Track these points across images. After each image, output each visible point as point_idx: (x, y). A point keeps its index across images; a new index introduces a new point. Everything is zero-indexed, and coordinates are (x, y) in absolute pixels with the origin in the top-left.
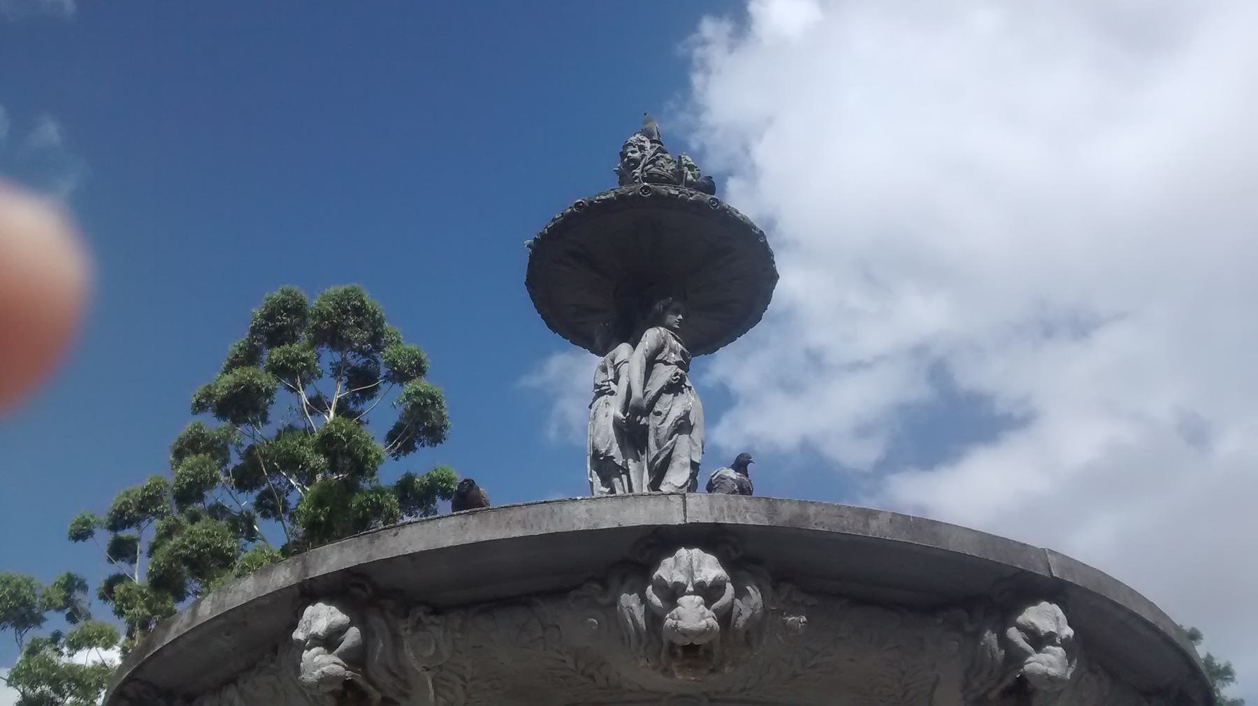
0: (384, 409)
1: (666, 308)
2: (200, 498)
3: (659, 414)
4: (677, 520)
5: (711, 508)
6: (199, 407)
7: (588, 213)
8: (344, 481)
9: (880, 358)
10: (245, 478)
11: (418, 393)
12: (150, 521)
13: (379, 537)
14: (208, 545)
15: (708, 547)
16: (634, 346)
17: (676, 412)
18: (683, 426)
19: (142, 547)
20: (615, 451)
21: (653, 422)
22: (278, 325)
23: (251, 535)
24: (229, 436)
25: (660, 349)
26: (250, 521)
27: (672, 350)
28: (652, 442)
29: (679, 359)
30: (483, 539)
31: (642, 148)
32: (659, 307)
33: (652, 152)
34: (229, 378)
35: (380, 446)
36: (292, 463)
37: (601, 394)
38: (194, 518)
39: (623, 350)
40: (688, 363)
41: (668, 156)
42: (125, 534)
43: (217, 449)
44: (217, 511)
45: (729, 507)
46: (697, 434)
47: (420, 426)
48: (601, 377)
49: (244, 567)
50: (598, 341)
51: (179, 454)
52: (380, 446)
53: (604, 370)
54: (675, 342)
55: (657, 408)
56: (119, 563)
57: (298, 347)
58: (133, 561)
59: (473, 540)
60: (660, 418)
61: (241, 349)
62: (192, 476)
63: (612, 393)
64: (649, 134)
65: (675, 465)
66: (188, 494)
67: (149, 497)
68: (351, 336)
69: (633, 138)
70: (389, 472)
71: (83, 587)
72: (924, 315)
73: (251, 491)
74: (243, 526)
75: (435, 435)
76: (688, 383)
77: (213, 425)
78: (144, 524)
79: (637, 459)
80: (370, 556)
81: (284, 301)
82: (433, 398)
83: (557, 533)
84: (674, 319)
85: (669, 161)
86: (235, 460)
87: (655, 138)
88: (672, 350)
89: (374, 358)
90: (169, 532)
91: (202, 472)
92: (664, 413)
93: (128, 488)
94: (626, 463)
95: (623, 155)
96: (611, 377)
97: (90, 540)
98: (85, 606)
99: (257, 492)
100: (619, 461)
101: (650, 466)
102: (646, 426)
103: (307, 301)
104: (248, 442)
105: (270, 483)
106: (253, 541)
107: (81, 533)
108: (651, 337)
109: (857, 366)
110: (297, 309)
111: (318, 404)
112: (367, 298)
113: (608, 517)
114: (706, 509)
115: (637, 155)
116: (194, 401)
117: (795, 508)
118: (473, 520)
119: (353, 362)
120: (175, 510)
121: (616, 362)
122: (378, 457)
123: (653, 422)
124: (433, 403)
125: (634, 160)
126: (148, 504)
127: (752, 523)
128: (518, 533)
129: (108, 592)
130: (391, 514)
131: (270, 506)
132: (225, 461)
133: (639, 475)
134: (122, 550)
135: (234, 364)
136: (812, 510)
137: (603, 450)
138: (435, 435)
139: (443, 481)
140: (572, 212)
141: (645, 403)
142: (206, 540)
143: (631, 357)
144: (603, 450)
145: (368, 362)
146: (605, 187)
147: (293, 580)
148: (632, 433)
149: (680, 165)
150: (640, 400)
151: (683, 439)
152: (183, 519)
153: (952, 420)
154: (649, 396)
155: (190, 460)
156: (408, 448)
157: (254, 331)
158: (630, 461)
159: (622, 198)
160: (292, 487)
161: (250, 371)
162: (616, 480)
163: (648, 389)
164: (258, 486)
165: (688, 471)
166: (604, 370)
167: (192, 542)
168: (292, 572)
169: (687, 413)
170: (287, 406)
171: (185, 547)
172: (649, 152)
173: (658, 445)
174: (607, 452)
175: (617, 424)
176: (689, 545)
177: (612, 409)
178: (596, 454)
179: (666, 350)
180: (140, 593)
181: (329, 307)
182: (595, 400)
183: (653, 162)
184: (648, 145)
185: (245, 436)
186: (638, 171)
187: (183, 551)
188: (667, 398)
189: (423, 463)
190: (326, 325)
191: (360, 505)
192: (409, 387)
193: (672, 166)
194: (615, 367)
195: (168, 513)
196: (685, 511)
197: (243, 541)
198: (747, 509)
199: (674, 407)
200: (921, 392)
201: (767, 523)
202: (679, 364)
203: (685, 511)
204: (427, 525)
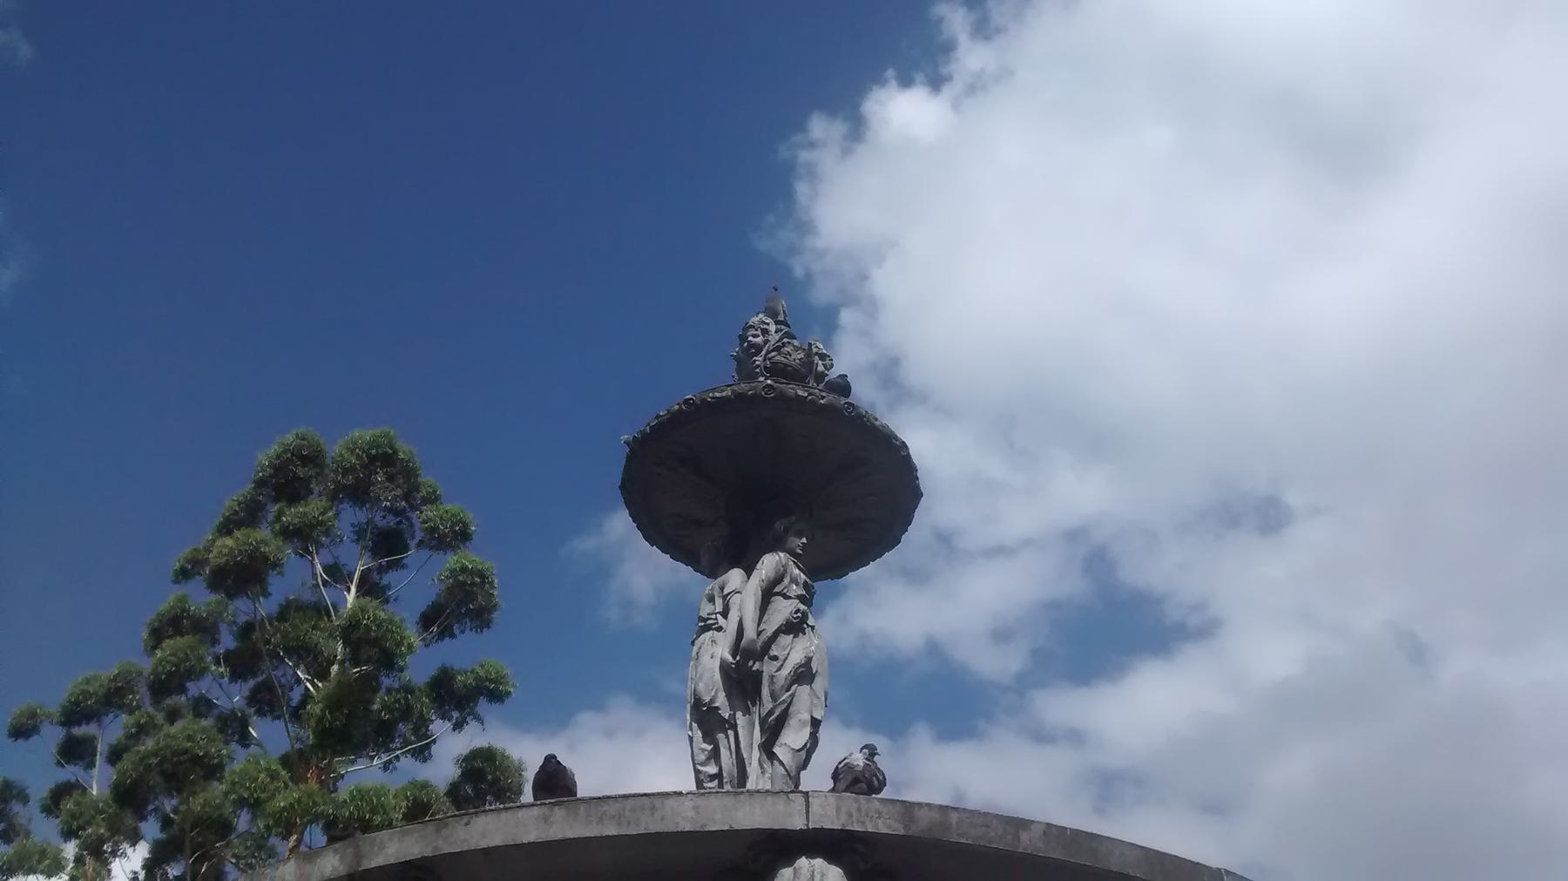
0: (419, 580)
1: (787, 530)
2: (182, 690)
3: (775, 658)
4: (798, 823)
5: (838, 810)
6: (184, 575)
7: (697, 413)
8: (367, 674)
9: (1027, 543)
10: (241, 664)
11: (464, 569)
13: (447, 825)
14: (186, 752)
15: (832, 858)
16: (749, 572)
17: (796, 657)
18: (804, 674)
19: (101, 748)
20: (721, 701)
21: (768, 668)
22: (288, 480)
23: (245, 740)
24: (221, 613)
25: (779, 579)
26: (244, 724)
27: (794, 581)
28: (765, 692)
29: (801, 592)
30: (570, 835)
31: (765, 332)
32: (779, 526)
35: (413, 635)
36: (306, 653)
37: (707, 628)
38: (173, 716)
39: (735, 577)
40: (812, 595)
41: (796, 343)
42: (79, 731)
43: (205, 629)
44: (202, 706)
45: (859, 810)
46: (819, 684)
47: (463, 606)
49: (234, 783)
50: (705, 561)
51: (157, 636)
52: (413, 635)
53: (711, 599)
54: (797, 571)
55: (774, 651)
56: (70, 768)
57: (314, 507)
58: (91, 765)
59: (559, 836)
60: (777, 664)
63: (720, 629)
64: (773, 314)
65: (793, 722)
66: (165, 685)
67: (118, 690)
68: (384, 498)
69: (755, 320)
70: (421, 663)
71: (24, 799)
72: (1082, 493)
73: (245, 680)
75: (482, 617)
76: (811, 621)
77: (200, 598)
78: (107, 720)
79: (747, 712)
80: (436, 848)
81: (300, 448)
82: (482, 575)
83: (658, 833)
84: (799, 542)
85: (797, 349)
86: (227, 641)
87: (781, 318)
88: (794, 581)
89: (408, 519)
90: (141, 731)
91: (187, 659)
92: (782, 658)
93: (90, 673)
94: (733, 716)
95: (743, 338)
96: (719, 608)
97: (34, 739)
98: (23, 821)
99: (252, 683)
100: (726, 713)
101: (763, 722)
102: (760, 673)
103: (326, 448)
104: (242, 619)
105: (268, 671)
106: (246, 746)
107: (22, 730)
108: (769, 564)
109: (1000, 551)
110: (309, 456)
111: (337, 574)
112: (399, 444)
113: (718, 816)
114: (832, 811)
115: (759, 340)
116: (178, 565)
117: (935, 815)
118: (559, 813)
119: (381, 523)
120: (147, 701)
122: (410, 647)
123: (768, 668)
124: (483, 583)
126: (114, 697)
127: (884, 831)
128: (611, 830)
129: (53, 805)
130: (421, 716)
131: (266, 700)
132: (215, 642)
133: (749, 732)
134: (75, 751)
135: (226, 528)
136: (954, 818)
137: (707, 699)
138: (482, 617)
139: (492, 681)
140: (680, 410)
141: (759, 644)
143: (743, 587)
144: (707, 699)
145: (400, 522)
146: (719, 380)
147: (342, 870)
148: (742, 679)
149: (809, 353)
150: (753, 641)
151: (803, 691)
152: (160, 718)
153: (1109, 623)
154: (764, 637)
155: (168, 644)
156: (446, 633)
157: (260, 484)
158: (739, 714)
159: (740, 397)
160: (299, 681)
162: (721, 736)
164: (254, 675)
165: (807, 730)
166: (711, 599)
168: (342, 860)
169: (809, 660)
170: (297, 576)
172: (774, 338)
173: (774, 697)
174: (712, 701)
175: (724, 667)
176: (811, 854)
177: (716, 650)
178: (697, 703)
179: (786, 581)
183: (777, 349)
184: (772, 328)
185: (241, 609)
186: (759, 359)
188: (785, 640)
189: (465, 653)
191: (385, 707)
192: (452, 560)
194: (724, 597)
195: (138, 707)
196: (807, 813)
197: (234, 746)
198: (880, 814)
199: (794, 651)
200: (1074, 586)
201: (902, 832)
202: (801, 598)
203: (807, 813)
204: (504, 815)
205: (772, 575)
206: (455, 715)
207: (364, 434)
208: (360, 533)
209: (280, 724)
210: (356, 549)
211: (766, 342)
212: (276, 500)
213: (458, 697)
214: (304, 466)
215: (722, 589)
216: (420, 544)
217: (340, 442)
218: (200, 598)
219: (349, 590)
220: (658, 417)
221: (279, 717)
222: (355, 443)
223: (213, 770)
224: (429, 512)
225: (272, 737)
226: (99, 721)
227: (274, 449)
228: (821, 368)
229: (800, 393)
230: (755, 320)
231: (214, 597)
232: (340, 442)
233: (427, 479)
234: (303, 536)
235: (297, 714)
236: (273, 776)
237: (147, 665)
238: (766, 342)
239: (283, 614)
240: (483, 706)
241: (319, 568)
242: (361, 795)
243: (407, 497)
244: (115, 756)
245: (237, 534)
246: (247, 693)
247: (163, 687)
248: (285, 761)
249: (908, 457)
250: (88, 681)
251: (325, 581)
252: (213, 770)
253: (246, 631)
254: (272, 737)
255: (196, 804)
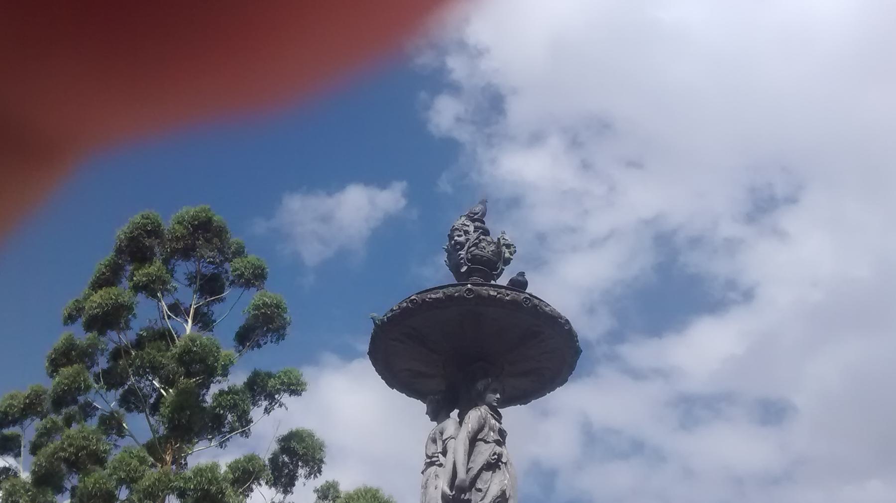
2: (75, 402)
3: (480, 490)
6: (70, 319)
10: (111, 379)
11: (265, 304)
12: (33, 420)
14: (84, 448)
22: (135, 249)
23: (121, 432)
25: (481, 429)
27: (491, 429)
29: (497, 437)
32: (480, 386)
33: (475, 236)
34: (97, 298)
35: (228, 350)
37: (430, 464)
38: (68, 422)
41: (489, 239)
43: (86, 356)
48: (432, 449)
49: (115, 468)
51: (55, 364)
52: (228, 350)
55: (479, 485)
57: (155, 267)
61: (106, 267)
62: (66, 385)
63: (441, 465)
67: (31, 403)
74: (112, 425)
77: (82, 337)
81: (145, 225)
85: (489, 243)
86: (103, 363)
88: (491, 429)
92: (484, 490)
93: (13, 392)
95: (451, 237)
96: (440, 450)
99: (121, 391)
104: (111, 346)
106: (123, 437)
110: (155, 232)
121: (444, 437)
125: (457, 243)
131: (131, 401)
135: (100, 284)
140: (408, 306)
142: (84, 443)
150: (464, 481)
155: (66, 371)
157: (119, 251)
160: (155, 390)
161: (114, 290)
163: (471, 465)
164: (122, 384)
167: (70, 445)
170: (147, 313)
171: (64, 450)
172: (473, 236)
179: (486, 430)
180: (24, 487)
181: (180, 230)
182: (425, 470)
183: (476, 245)
185: (113, 339)
186: (463, 253)
187: (62, 454)
188: (487, 475)
189: (267, 357)
190: (181, 245)
192: (254, 297)
193: (493, 248)
194: (444, 441)
205: (476, 427)
206: (265, 403)
207: (188, 211)
208: (191, 279)
209: (143, 415)
210: (190, 290)
211: (468, 240)
212: (132, 262)
213: (261, 388)
214: (149, 237)
215: (442, 434)
216: (232, 283)
217: (173, 216)
218: (82, 337)
219: (187, 321)
220: (392, 310)
221: (141, 412)
222: (183, 218)
223: (99, 460)
224: (238, 263)
225: (140, 427)
226: (22, 424)
227: (125, 228)
228: (507, 255)
229: (492, 293)
230: (458, 223)
231: (89, 335)
232: (173, 216)
233: (234, 239)
234: (149, 288)
235: (155, 409)
236: (142, 461)
237: (49, 385)
238: (468, 240)
239: (139, 344)
240: (285, 398)
241: (165, 308)
242: (199, 472)
243: (221, 251)
244: (35, 449)
245: (100, 292)
246: (119, 397)
247: (60, 401)
248: (150, 448)
249: (571, 329)
250: (12, 397)
251: (166, 313)
252: (99, 460)
253: (116, 355)
254: (140, 427)
255: (90, 481)
